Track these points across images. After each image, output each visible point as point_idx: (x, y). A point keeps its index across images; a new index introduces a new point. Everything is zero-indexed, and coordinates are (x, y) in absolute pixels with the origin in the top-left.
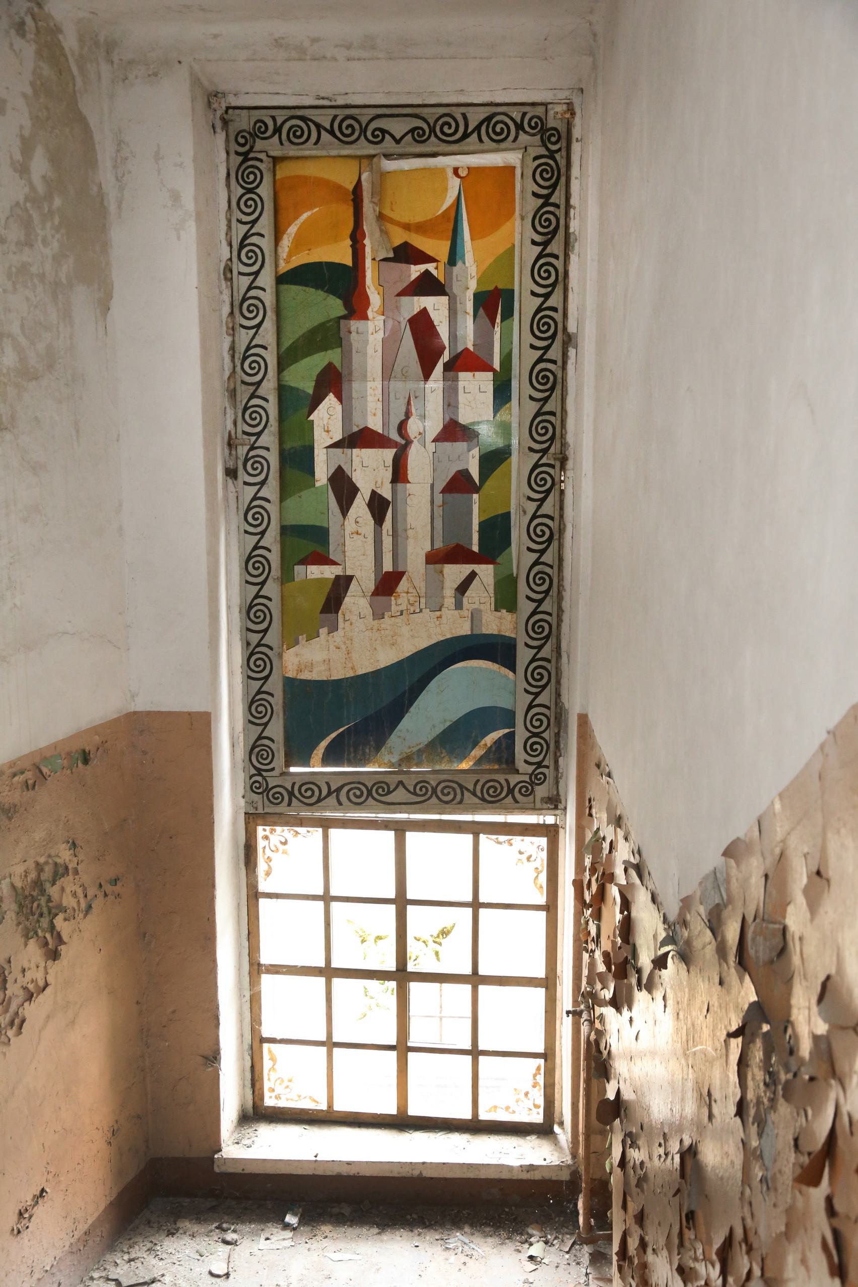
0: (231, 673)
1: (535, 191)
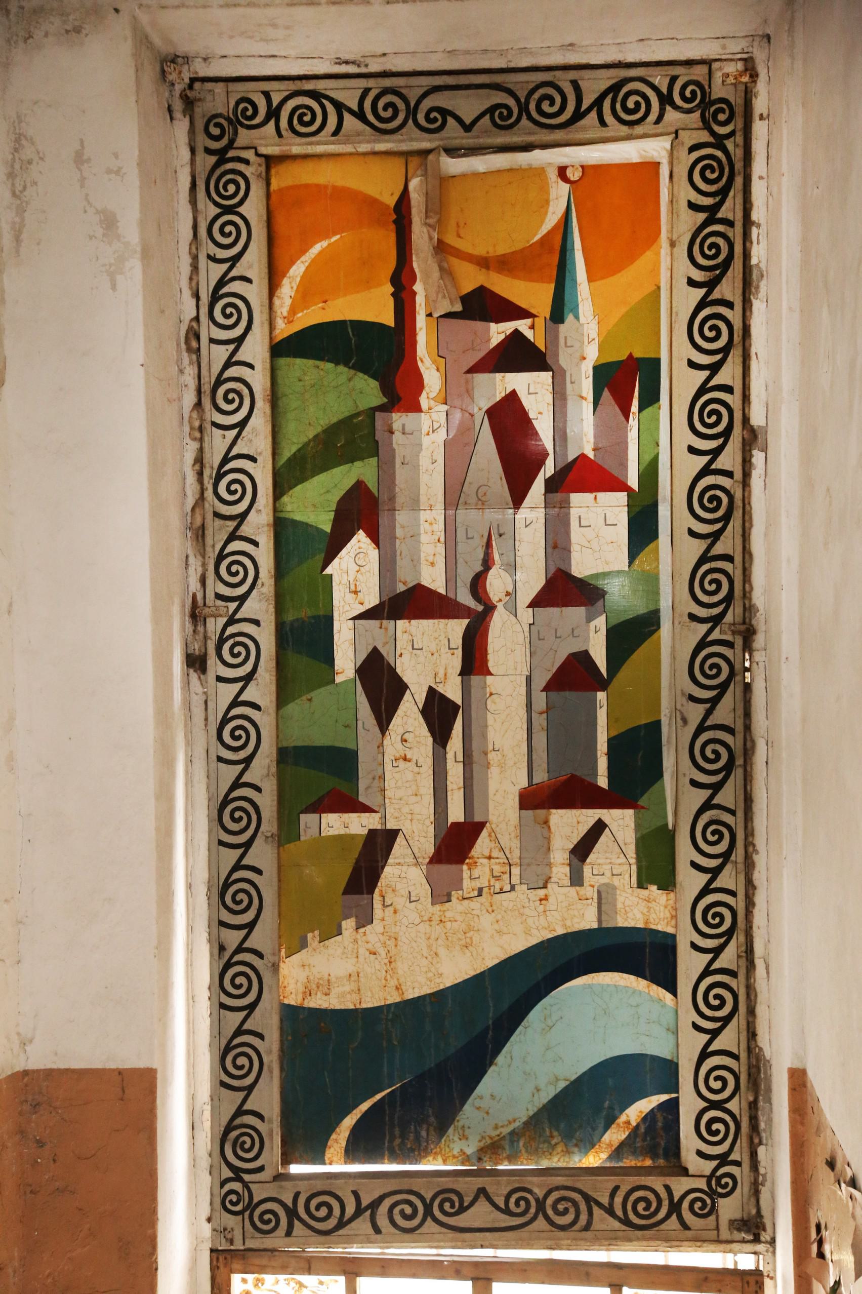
0: (191, 999)
1: (693, 201)
